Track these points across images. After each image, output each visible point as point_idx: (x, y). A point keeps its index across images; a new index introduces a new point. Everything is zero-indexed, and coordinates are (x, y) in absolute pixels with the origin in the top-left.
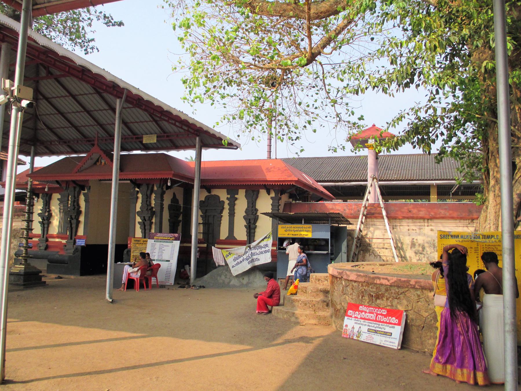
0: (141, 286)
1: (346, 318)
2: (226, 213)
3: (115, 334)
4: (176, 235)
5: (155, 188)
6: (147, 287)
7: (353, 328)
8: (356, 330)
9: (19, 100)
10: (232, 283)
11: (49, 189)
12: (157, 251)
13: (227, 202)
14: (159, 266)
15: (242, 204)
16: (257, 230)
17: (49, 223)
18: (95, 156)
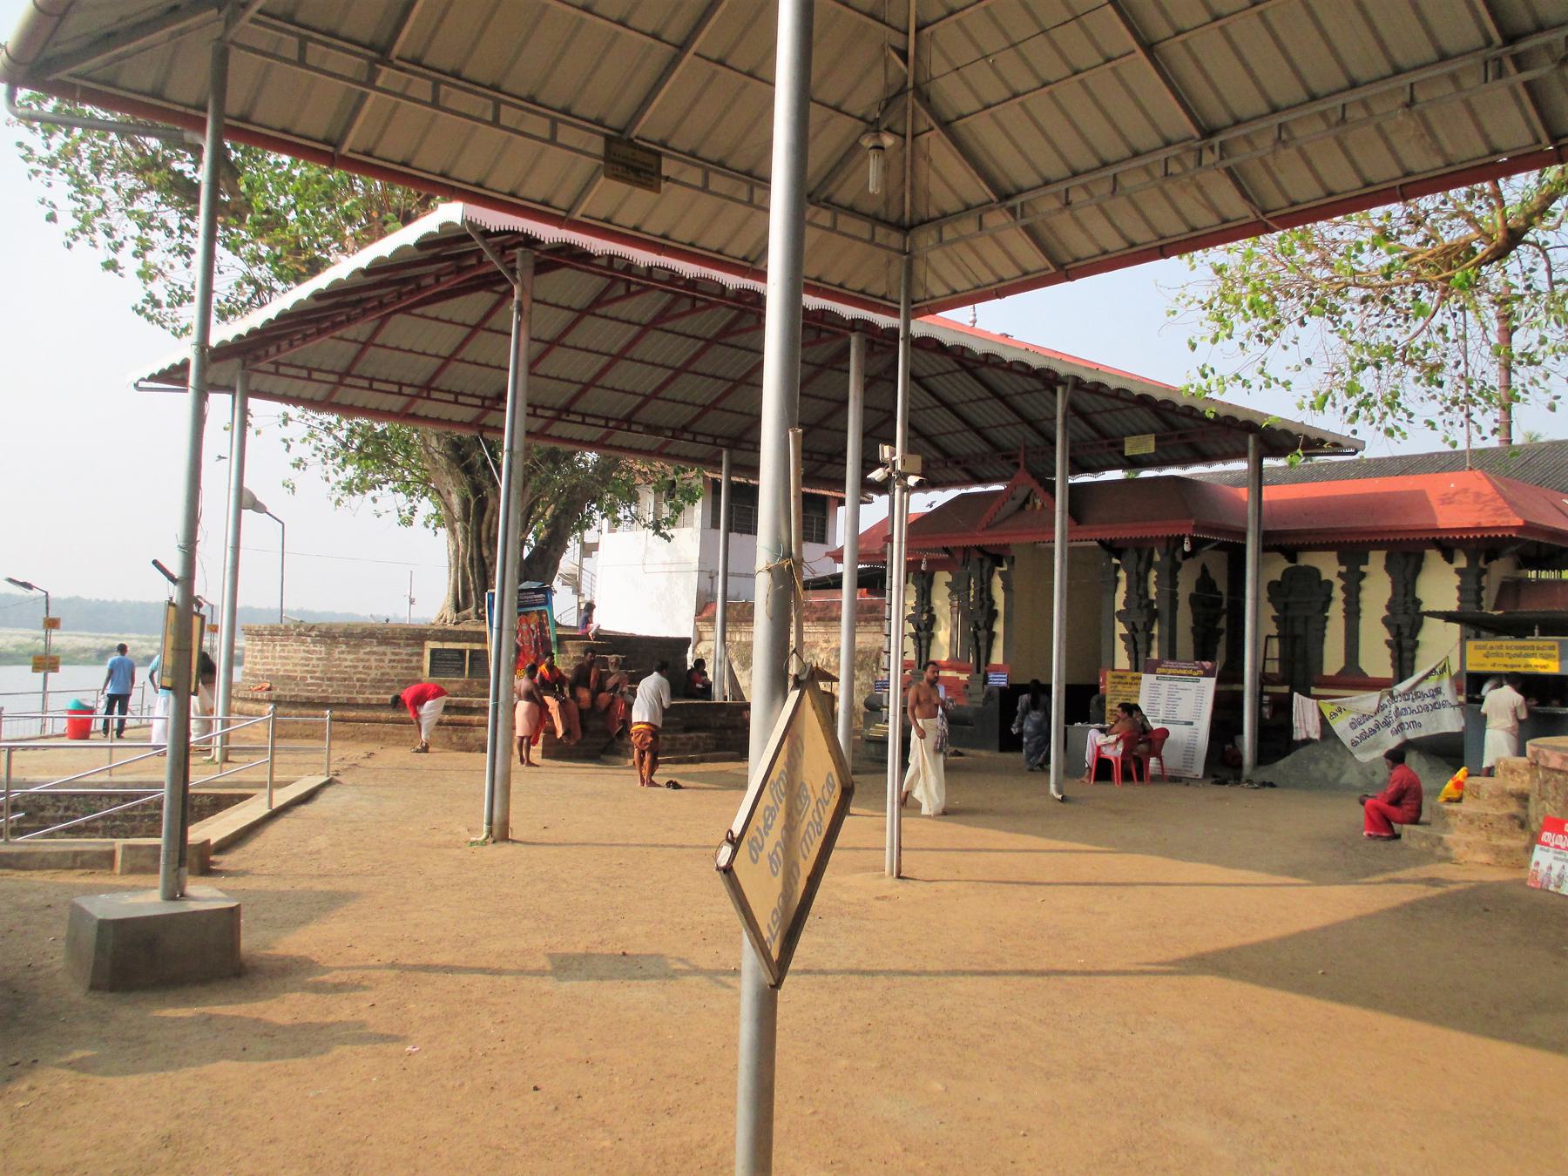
0: (1127, 777)
1: (1537, 847)
2: (1336, 611)
3: (1062, 845)
4: (1207, 664)
5: (1157, 557)
6: (1140, 779)
7: (1550, 868)
8: (1554, 874)
9: (904, 476)
10: (1344, 780)
11: (929, 562)
12: (1162, 700)
13: (1338, 584)
14: (1165, 733)
15: (1377, 590)
16: (1420, 652)
17: (931, 637)
18: (1021, 493)
